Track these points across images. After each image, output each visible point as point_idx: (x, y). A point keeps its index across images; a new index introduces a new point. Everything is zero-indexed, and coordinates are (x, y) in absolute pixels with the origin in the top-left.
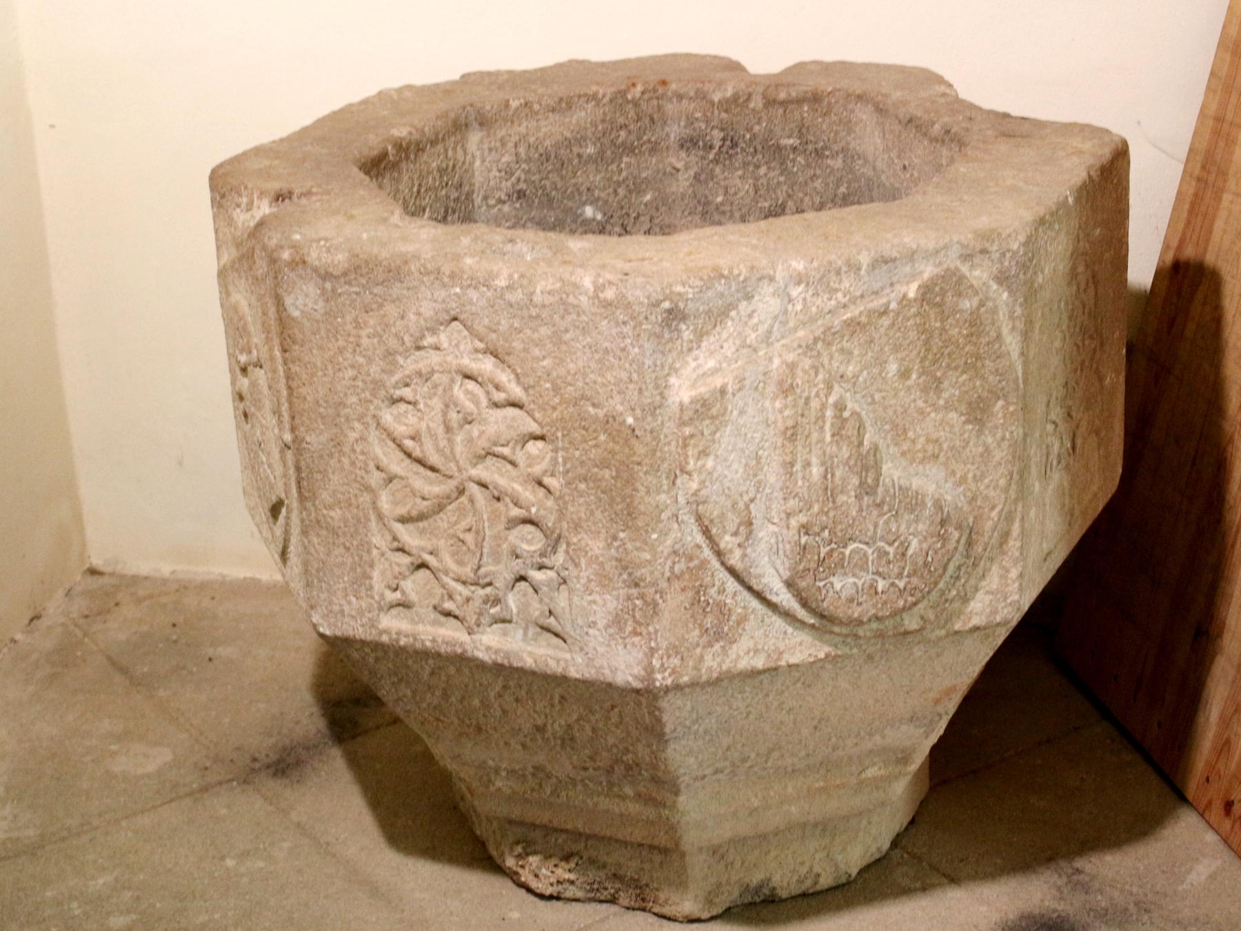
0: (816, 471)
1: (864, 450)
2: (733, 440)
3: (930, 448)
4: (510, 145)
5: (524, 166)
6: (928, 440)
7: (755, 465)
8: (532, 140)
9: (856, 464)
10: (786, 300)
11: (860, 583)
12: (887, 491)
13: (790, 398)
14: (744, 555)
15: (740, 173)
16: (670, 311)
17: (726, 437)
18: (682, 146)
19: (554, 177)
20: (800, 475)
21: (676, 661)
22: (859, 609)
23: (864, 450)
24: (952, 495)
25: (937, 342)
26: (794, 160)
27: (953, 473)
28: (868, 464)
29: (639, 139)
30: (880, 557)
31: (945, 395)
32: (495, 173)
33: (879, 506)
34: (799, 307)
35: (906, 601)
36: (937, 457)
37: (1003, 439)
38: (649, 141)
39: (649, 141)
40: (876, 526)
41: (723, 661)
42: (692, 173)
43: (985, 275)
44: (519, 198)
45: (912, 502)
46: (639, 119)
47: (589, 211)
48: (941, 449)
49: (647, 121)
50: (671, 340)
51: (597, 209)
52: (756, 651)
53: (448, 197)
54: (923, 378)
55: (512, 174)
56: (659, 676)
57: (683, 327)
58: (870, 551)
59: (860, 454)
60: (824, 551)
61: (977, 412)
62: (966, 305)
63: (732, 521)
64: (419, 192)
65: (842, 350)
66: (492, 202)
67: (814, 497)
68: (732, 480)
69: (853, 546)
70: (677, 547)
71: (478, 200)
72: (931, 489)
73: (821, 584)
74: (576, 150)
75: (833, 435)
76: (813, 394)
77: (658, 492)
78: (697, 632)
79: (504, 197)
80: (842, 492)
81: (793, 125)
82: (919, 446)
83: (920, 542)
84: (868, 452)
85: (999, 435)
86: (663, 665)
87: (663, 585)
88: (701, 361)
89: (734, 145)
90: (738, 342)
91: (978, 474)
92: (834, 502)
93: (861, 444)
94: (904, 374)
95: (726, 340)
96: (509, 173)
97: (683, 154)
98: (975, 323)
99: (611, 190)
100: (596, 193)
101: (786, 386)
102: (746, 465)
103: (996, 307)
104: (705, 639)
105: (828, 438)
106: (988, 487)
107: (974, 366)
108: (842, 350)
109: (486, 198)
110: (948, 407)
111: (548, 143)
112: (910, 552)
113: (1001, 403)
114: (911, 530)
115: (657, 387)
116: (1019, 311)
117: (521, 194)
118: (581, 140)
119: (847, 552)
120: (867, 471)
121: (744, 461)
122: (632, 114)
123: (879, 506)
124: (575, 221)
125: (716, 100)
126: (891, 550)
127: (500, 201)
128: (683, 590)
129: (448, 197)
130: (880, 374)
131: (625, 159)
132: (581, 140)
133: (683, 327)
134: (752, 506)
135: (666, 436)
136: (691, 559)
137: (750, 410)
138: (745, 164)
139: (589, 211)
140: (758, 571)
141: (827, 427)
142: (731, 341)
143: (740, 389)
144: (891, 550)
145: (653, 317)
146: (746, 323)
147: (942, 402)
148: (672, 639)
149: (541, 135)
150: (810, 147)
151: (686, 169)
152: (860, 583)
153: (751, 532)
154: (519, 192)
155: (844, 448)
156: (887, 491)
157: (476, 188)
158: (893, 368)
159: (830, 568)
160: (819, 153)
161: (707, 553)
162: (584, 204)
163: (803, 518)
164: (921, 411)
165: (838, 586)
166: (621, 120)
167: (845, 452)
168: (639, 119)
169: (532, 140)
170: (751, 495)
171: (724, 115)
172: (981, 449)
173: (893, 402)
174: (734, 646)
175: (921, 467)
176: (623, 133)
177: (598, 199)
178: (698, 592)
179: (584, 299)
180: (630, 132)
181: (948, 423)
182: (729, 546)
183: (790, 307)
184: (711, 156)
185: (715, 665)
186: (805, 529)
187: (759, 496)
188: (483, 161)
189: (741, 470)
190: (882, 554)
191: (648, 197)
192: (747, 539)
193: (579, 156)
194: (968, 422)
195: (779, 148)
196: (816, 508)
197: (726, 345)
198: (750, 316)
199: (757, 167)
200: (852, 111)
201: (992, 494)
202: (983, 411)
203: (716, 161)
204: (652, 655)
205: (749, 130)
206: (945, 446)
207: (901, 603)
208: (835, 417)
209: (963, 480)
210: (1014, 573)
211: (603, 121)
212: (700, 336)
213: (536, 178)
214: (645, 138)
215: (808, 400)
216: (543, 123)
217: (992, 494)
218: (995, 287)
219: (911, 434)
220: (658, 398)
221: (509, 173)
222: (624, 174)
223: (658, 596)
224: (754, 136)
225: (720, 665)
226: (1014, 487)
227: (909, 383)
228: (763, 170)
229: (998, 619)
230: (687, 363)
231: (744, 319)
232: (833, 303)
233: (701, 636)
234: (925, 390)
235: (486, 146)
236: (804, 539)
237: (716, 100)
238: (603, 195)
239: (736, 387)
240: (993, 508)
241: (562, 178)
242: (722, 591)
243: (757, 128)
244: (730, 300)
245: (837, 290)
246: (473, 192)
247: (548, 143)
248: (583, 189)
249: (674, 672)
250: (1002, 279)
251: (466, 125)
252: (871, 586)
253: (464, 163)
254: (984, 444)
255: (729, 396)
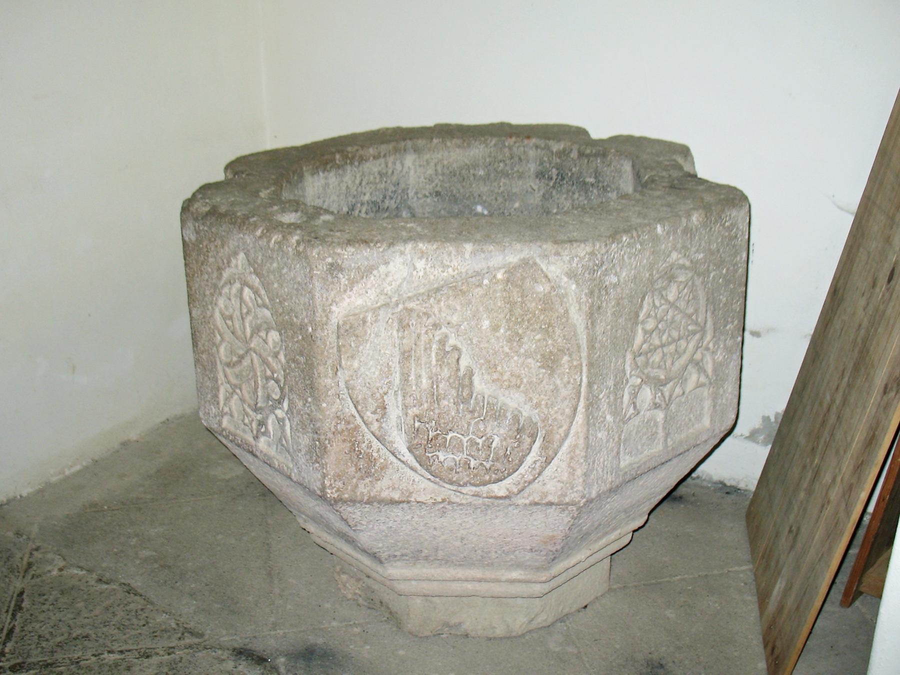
0: (425, 382)
1: (461, 373)
2: (371, 353)
3: (514, 380)
4: (432, 164)
5: (441, 177)
6: (512, 375)
7: (387, 372)
8: (445, 162)
9: (454, 382)
10: (412, 269)
11: (458, 459)
12: (478, 403)
13: (406, 332)
14: (381, 427)
15: (565, 196)
16: (332, 265)
17: (366, 349)
18: (537, 177)
19: (459, 186)
20: (414, 382)
21: (340, 484)
22: (457, 476)
23: (461, 373)
24: (527, 411)
25: (518, 311)
26: (592, 192)
27: (531, 399)
28: (464, 383)
29: (512, 169)
30: (472, 446)
31: (525, 347)
32: (422, 179)
33: (472, 412)
34: (421, 274)
35: (491, 476)
36: (519, 387)
37: (569, 382)
38: (518, 171)
39: (518, 171)
40: (469, 424)
41: (371, 490)
42: (541, 193)
43: (559, 271)
44: (436, 196)
45: (497, 414)
46: (512, 158)
47: (479, 209)
48: (522, 382)
49: (517, 159)
50: (333, 283)
51: (484, 207)
52: (394, 489)
53: (386, 189)
54: (509, 333)
55: (433, 182)
56: (329, 491)
57: (341, 276)
58: (465, 440)
59: (457, 376)
60: (431, 434)
61: (550, 362)
62: (540, 288)
63: (372, 405)
64: (360, 184)
65: (449, 307)
66: (420, 196)
67: (424, 399)
68: (371, 378)
69: (451, 434)
70: (339, 413)
71: (411, 194)
72: (512, 404)
73: (430, 455)
74: (472, 171)
75: (437, 361)
76: (423, 332)
77: (326, 376)
78: (354, 469)
79: (427, 194)
80: (444, 399)
81: (592, 170)
82: (506, 377)
83: (501, 441)
84: (464, 375)
85: (566, 379)
86: (331, 485)
87: (330, 435)
88: (353, 299)
89: (563, 179)
90: (378, 291)
91: (549, 402)
92: (438, 404)
93: (458, 370)
94: (495, 328)
95: (370, 289)
96: (431, 180)
97: (537, 181)
98: (547, 303)
99: (493, 198)
100: (484, 198)
101: (404, 324)
102: (381, 370)
103: (566, 294)
104: (359, 475)
105: (434, 362)
106: (556, 412)
107: (547, 330)
108: (449, 307)
109: (416, 193)
110: (527, 355)
111: (455, 165)
112: (494, 445)
113: (566, 358)
114: (495, 432)
115: (324, 311)
116: (584, 299)
117: (438, 194)
118: (475, 166)
119: (448, 438)
120: (463, 389)
121: (379, 367)
122: (508, 154)
123: (472, 412)
124: (470, 213)
125: (554, 150)
126: (480, 441)
127: (425, 196)
128: (344, 441)
129: (386, 189)
130: (477, 325)
131: (503, 180)
132: (475, 166)
133: (341, 276)
134: (385, 397)
135: (330, 343)
136: (348, 423)
137: (383, 335)
138: (568, 191)
139: (479, 209)
140: (391, 439)
141: (433, 355)
142: (373, 289)
143: (376, 321)
144: (480, 441)
145: (320, 267)
146: (384, 279)
147: (522, 351)
148: (337, 471)
149: (451, 160)
150: (600, 185)
151: (539, 190)
152: (458, 459)
153: (385, 414)
154: (437, 192)
155: (446, 370)
156: (478, 403)
157: (410, 187)
158: (486, 324)
159: (436, 446)
160: (605, 189)
161: (359, 420)
162: (477, 204)
163: (416, 411)
164: (507, 355)
165: (442, 458)
166: (500, 157)
167: (446, 373)
168: (512, 158)
169: (445, 162)
170: (385, 390)
171: (558, 161)
172: (552, 387)
173: (486, 345)
174: (379, 482)
175: (507, 392)
176: (502, 165)
177: (485, 202)
178: (354, 445)
179: (290, 249)
180: (506, 165)
181: (527, 366)
182: (370, 420)
183: (415, 273)
184: (551, 184)
185: (365, 491)
186: (419, 418)
187: (390, 391)
188: (416, 172)
189: (377, 373)
190: (473, 443)
191: (517, 205)
192: (382, 417)
193: (474, 175)
194: (542, 367)
195: (585, 183)
196: (426, 406)
197: (369, 291)
198: (387, 275)
199: (574, 193)
200: (622, 165)
201: (560, 417)
202: (553, 362)
203: (554, 187)
204: (324, 478)
205: (571, 170)
206: (525, 380)
207: (487, 477)
208: (439, 349)
209: (538, 405)
210: (579, 472)
211: (490, 156)
212: (352, 283)
213: (447, 185)
214: (515, 169)
215: (419, 336)
216: (452, 154)
217: (560, 417)
218: (565, 279)
219: (499, 368)
220: (325, 319)
221: (431, 180)
222: (502, 189)
223: (327, 442)
224: (573, 174)
225: (369, 492)
226: (580, 418)
227: (497, 334)
228: (576, 196)
229: (567, 500)
230: (344, 299)
231: (383, 277)
232: (445, 274)
233: (356, 472)
234: (510, 340)
235: (417, 163)
236: (417, 424)
237: (554, 150)
238: (489, 200)
239: (374, 319)
240: (561, 427)
241: (463, 187)
242: (370, 446)
243: (574, 169)
244: (371, 263)
245: (448, 266)
246: (408, 189)
247: (455, 165)
248: (476, 195)
249: (338, 490)
250: (572, 275)
251: (405, 150)
252: (466, 463)
253: (401, 171)
254: (555, 384)
255: (368, 324)
